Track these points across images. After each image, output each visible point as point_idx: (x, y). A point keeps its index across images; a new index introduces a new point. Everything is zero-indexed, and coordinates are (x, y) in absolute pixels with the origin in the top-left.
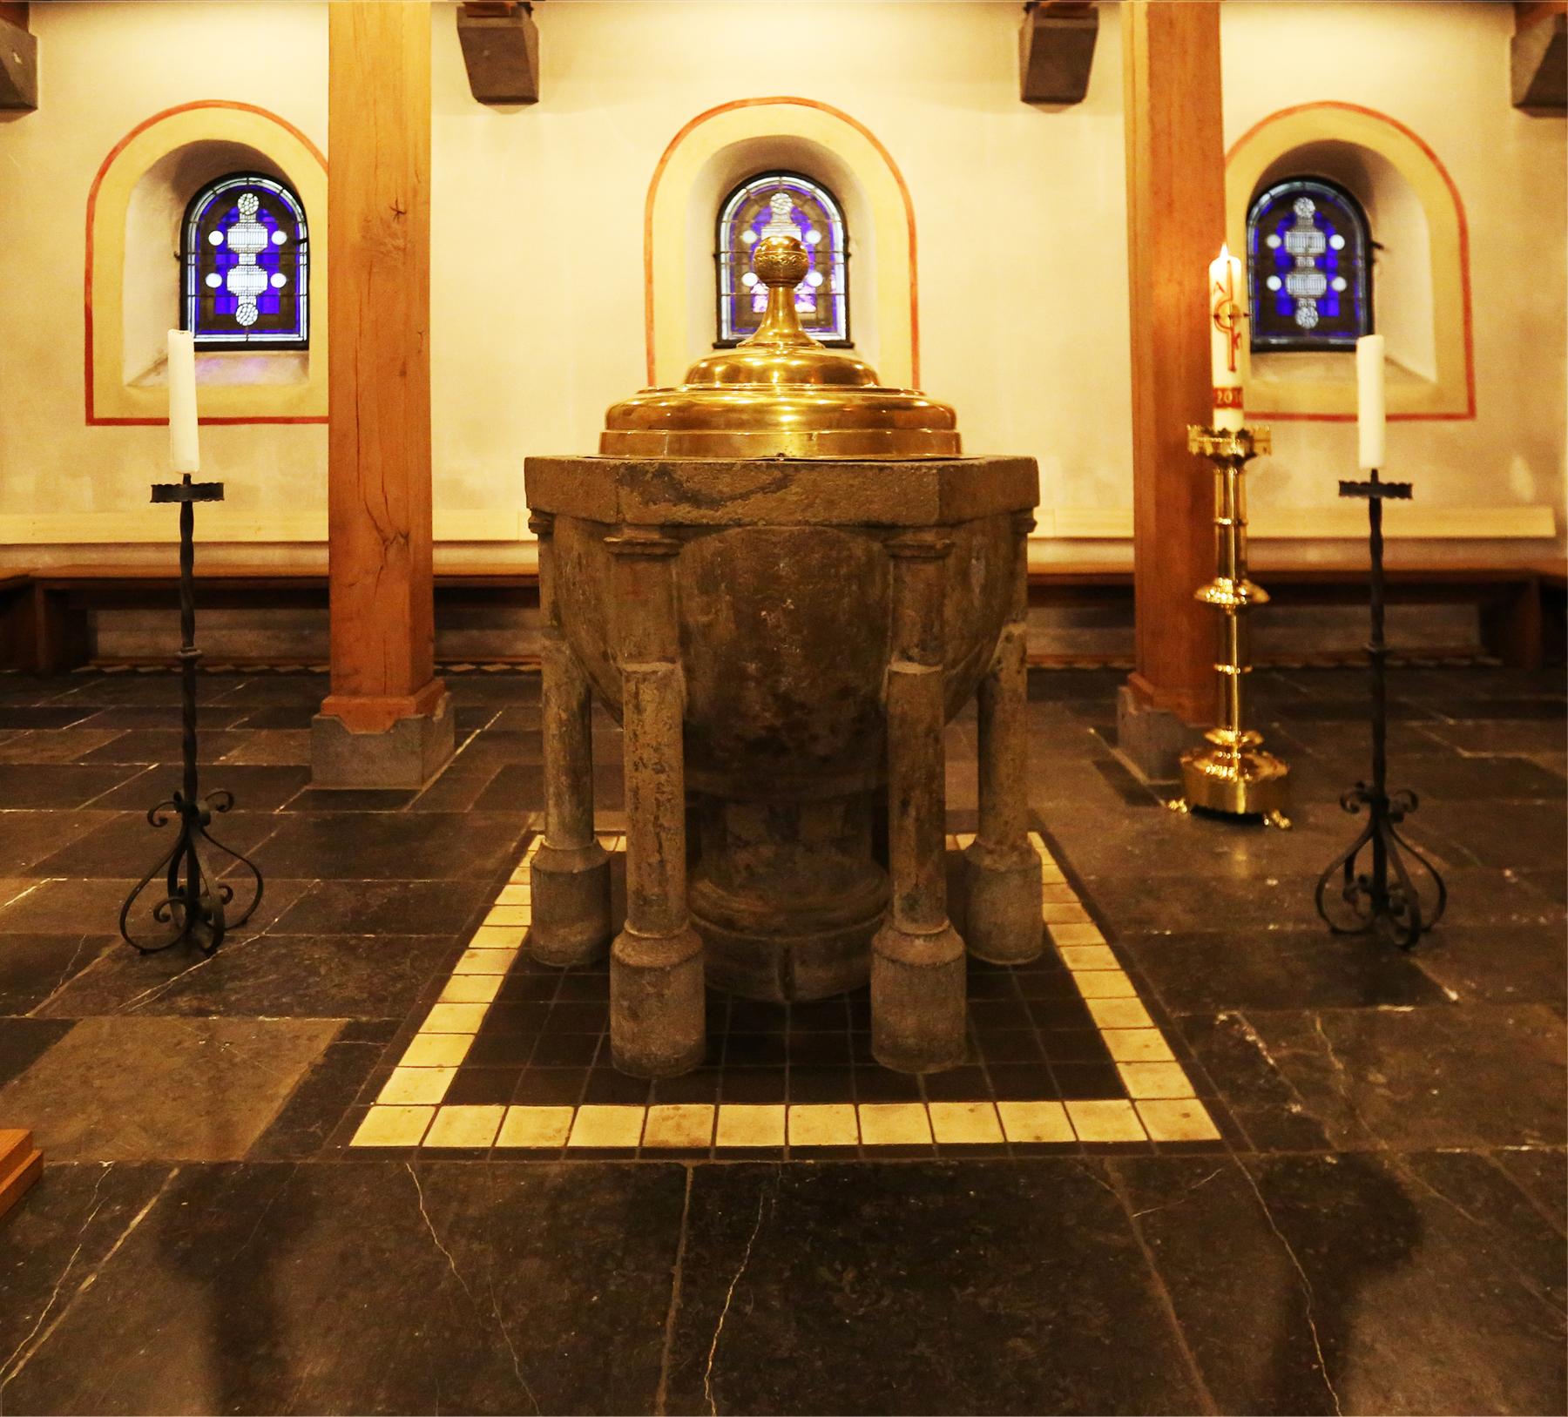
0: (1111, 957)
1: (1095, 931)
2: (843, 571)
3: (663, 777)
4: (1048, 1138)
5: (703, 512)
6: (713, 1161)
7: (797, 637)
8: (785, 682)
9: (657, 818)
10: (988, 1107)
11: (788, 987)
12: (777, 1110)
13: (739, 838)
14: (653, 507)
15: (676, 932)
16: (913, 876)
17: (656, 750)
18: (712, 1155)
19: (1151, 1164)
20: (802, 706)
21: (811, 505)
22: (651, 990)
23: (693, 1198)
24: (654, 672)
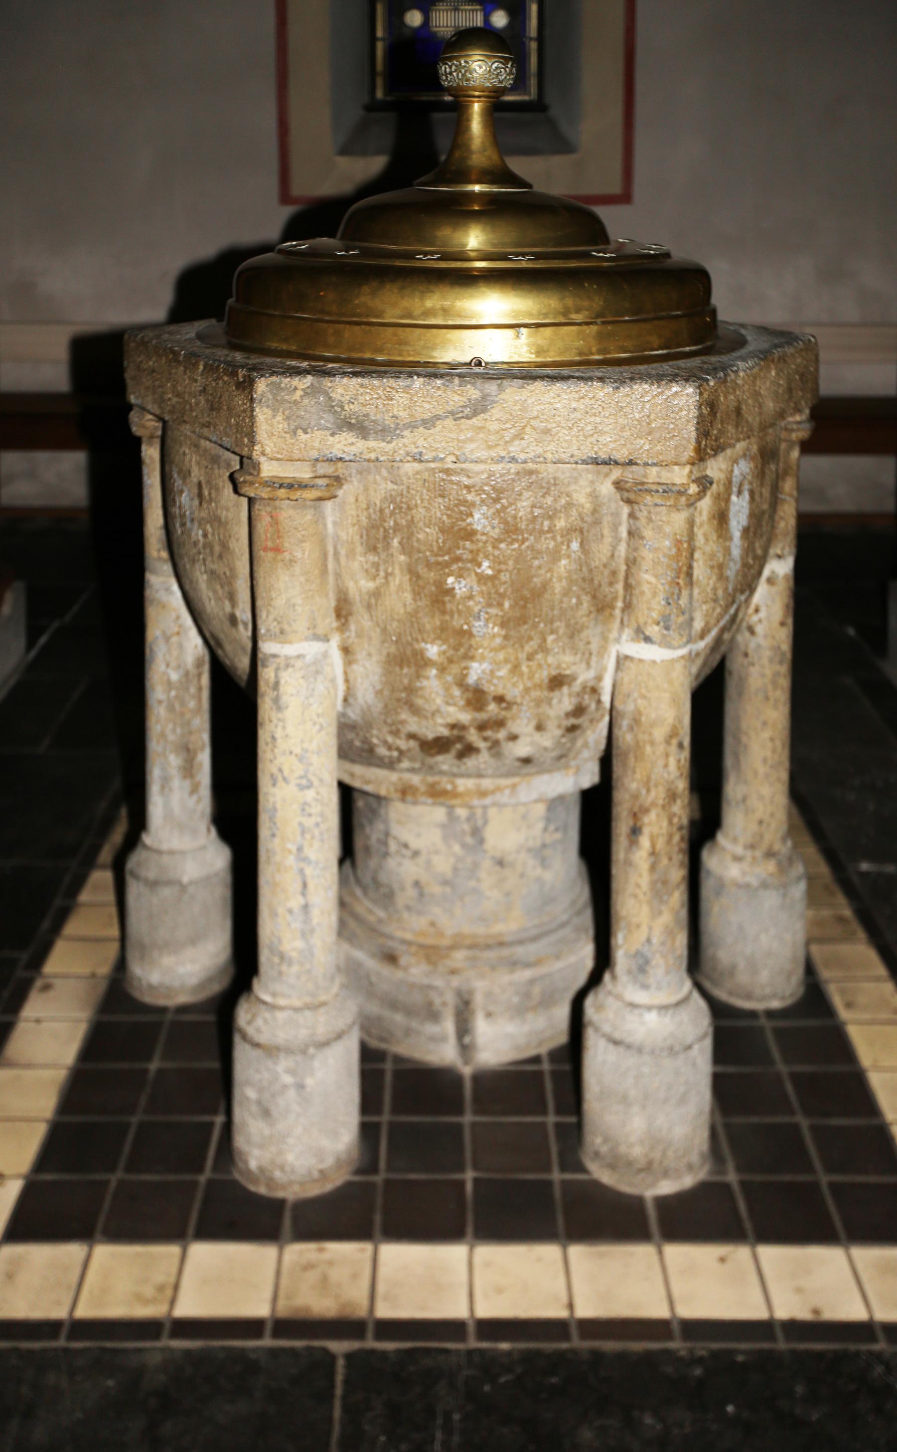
1: (871, 955)
2: (561, 523)
3: (310, 794)
5: (372, 444)
6: (371, 1344)
7: (493, 611)
9: (300, 849)
10: (741, 1253)
13: (406, 846)
14: (303, 437)
15: (323, 998)
17: (301, 759)
18: (370, 1333)
20: (500, 699)
21: (519, 436)
22: (288, 1079)
23: (346, 1408)
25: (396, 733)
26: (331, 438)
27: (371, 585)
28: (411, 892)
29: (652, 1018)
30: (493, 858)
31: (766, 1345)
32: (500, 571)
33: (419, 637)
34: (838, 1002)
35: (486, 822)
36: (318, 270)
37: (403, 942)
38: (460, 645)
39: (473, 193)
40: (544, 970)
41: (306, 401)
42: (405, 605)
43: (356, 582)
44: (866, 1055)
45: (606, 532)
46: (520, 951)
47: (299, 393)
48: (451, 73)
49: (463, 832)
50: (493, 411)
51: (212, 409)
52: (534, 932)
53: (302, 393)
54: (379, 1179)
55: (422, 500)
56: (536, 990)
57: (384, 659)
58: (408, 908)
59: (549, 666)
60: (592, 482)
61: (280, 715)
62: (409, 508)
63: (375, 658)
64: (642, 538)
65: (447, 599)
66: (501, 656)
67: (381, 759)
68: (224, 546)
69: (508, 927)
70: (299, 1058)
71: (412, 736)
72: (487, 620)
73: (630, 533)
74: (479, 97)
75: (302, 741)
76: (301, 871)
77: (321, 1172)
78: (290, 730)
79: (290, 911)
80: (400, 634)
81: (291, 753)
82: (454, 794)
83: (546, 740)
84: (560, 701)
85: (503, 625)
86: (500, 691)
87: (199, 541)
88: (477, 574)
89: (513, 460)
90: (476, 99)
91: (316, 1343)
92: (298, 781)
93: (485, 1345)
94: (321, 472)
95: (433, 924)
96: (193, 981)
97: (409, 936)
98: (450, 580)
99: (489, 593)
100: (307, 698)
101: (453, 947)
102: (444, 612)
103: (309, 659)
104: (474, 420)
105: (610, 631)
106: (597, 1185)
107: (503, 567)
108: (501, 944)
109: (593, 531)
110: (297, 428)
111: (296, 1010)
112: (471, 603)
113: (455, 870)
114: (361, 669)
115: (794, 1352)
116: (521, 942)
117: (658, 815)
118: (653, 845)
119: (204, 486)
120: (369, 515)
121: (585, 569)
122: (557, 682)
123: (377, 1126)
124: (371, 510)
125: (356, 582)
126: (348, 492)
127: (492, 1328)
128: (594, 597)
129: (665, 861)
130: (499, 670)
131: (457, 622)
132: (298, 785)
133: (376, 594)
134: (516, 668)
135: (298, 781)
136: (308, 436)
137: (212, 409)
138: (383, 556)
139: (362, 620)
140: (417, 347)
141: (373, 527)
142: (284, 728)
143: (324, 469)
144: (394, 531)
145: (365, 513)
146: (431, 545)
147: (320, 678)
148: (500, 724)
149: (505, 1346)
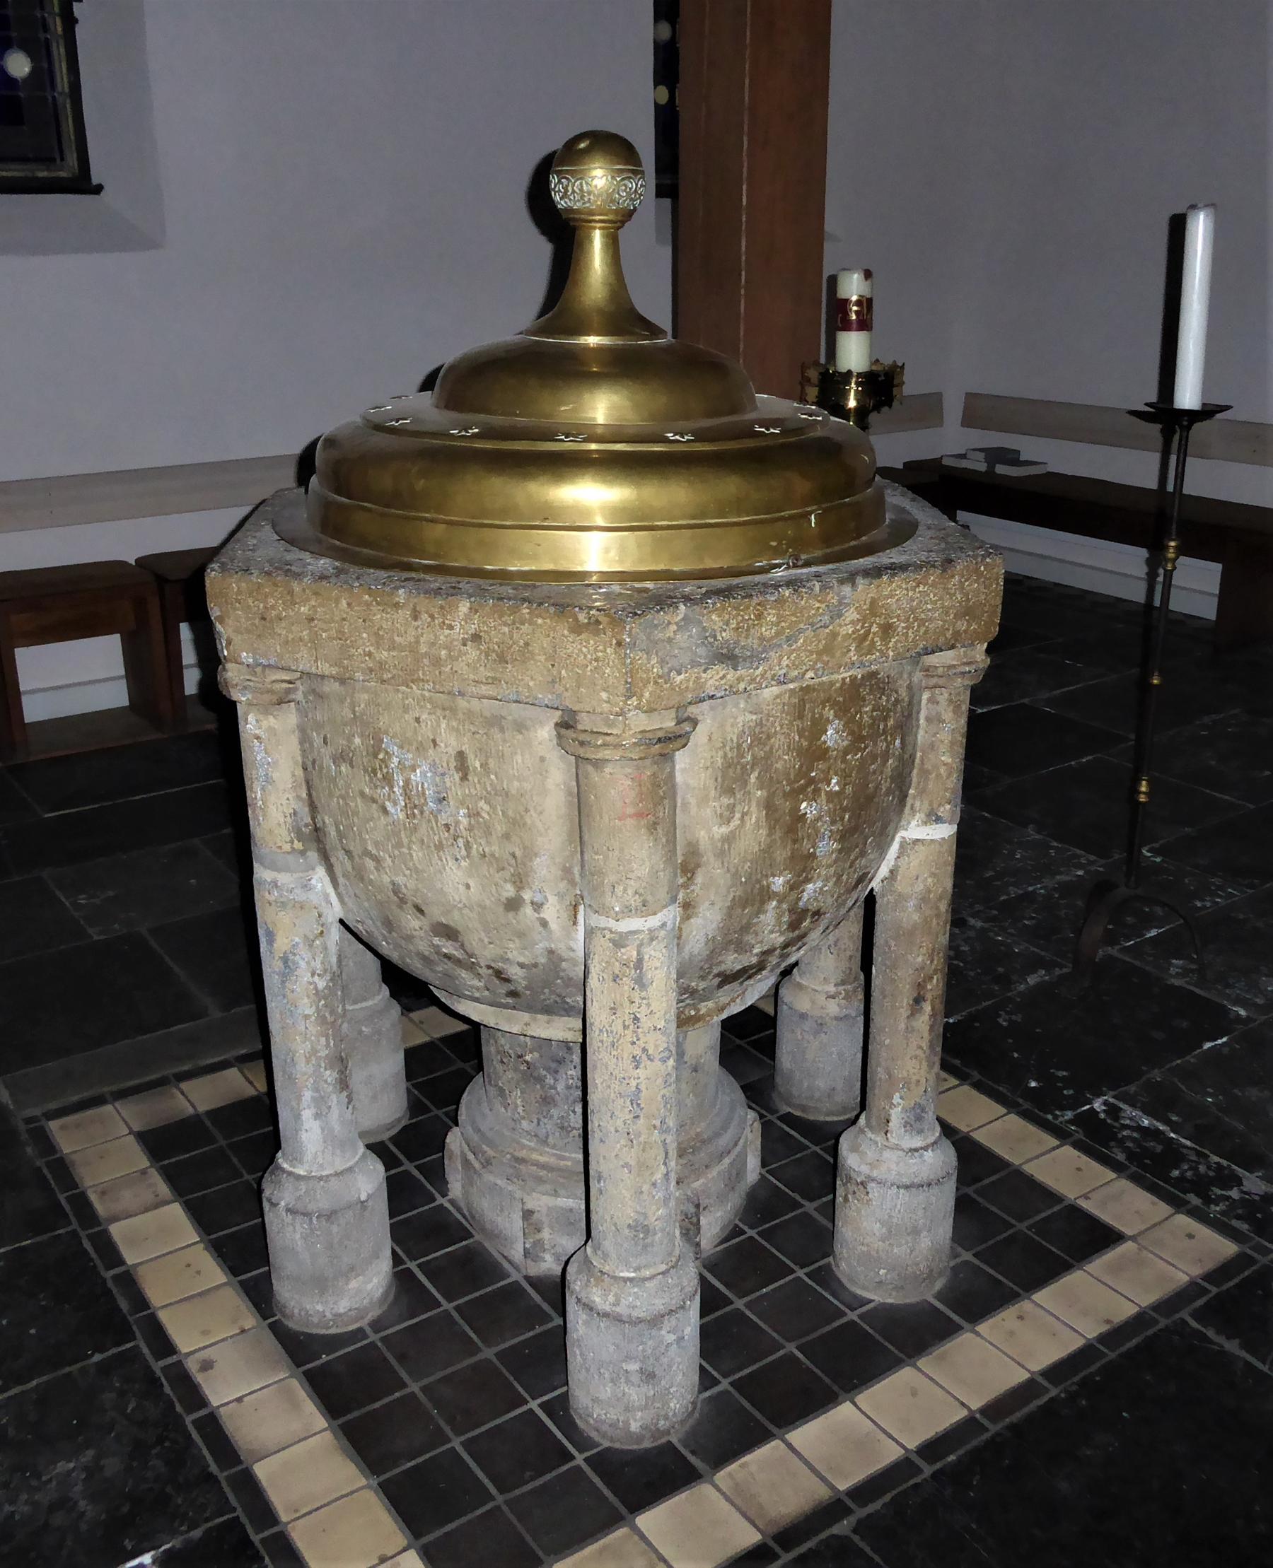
2: (891, 722)
10: (1025, 1305)
12: (844, 1411)
14: (679, 679)
19: (1248, 1298)
22: (671, 1338)
26: (704, 675)
27: (724, 830)
29: (929, 1155)
31: (1103, 1361)
36: (448, 458)
39: (586, 348)
51: (502, 659)
54: (725, 1384)
55: (781, 727)
61: (644, 994)
62: (769, 737)
63: (717, 907)
68: (516, 824)
81: (655, 1028)
89: (862, 665)
90: (598, 225)
93: (938, 1465)
96: (379, 1293)
98: (804, 805)
106: (885, 1309)
111: (663, 1273)
115: (1120, 1355)
116: (717, 1135)
120: (725, 754)
123: (159, 1356)
125: (709, 830)
126: (700, 736)
127: (931, 1449)
133: (729, 839)
136: (682, 676)
142: (648, 1005)
145: (721, 753)
146: (789, 774)
149: (952, 1458)
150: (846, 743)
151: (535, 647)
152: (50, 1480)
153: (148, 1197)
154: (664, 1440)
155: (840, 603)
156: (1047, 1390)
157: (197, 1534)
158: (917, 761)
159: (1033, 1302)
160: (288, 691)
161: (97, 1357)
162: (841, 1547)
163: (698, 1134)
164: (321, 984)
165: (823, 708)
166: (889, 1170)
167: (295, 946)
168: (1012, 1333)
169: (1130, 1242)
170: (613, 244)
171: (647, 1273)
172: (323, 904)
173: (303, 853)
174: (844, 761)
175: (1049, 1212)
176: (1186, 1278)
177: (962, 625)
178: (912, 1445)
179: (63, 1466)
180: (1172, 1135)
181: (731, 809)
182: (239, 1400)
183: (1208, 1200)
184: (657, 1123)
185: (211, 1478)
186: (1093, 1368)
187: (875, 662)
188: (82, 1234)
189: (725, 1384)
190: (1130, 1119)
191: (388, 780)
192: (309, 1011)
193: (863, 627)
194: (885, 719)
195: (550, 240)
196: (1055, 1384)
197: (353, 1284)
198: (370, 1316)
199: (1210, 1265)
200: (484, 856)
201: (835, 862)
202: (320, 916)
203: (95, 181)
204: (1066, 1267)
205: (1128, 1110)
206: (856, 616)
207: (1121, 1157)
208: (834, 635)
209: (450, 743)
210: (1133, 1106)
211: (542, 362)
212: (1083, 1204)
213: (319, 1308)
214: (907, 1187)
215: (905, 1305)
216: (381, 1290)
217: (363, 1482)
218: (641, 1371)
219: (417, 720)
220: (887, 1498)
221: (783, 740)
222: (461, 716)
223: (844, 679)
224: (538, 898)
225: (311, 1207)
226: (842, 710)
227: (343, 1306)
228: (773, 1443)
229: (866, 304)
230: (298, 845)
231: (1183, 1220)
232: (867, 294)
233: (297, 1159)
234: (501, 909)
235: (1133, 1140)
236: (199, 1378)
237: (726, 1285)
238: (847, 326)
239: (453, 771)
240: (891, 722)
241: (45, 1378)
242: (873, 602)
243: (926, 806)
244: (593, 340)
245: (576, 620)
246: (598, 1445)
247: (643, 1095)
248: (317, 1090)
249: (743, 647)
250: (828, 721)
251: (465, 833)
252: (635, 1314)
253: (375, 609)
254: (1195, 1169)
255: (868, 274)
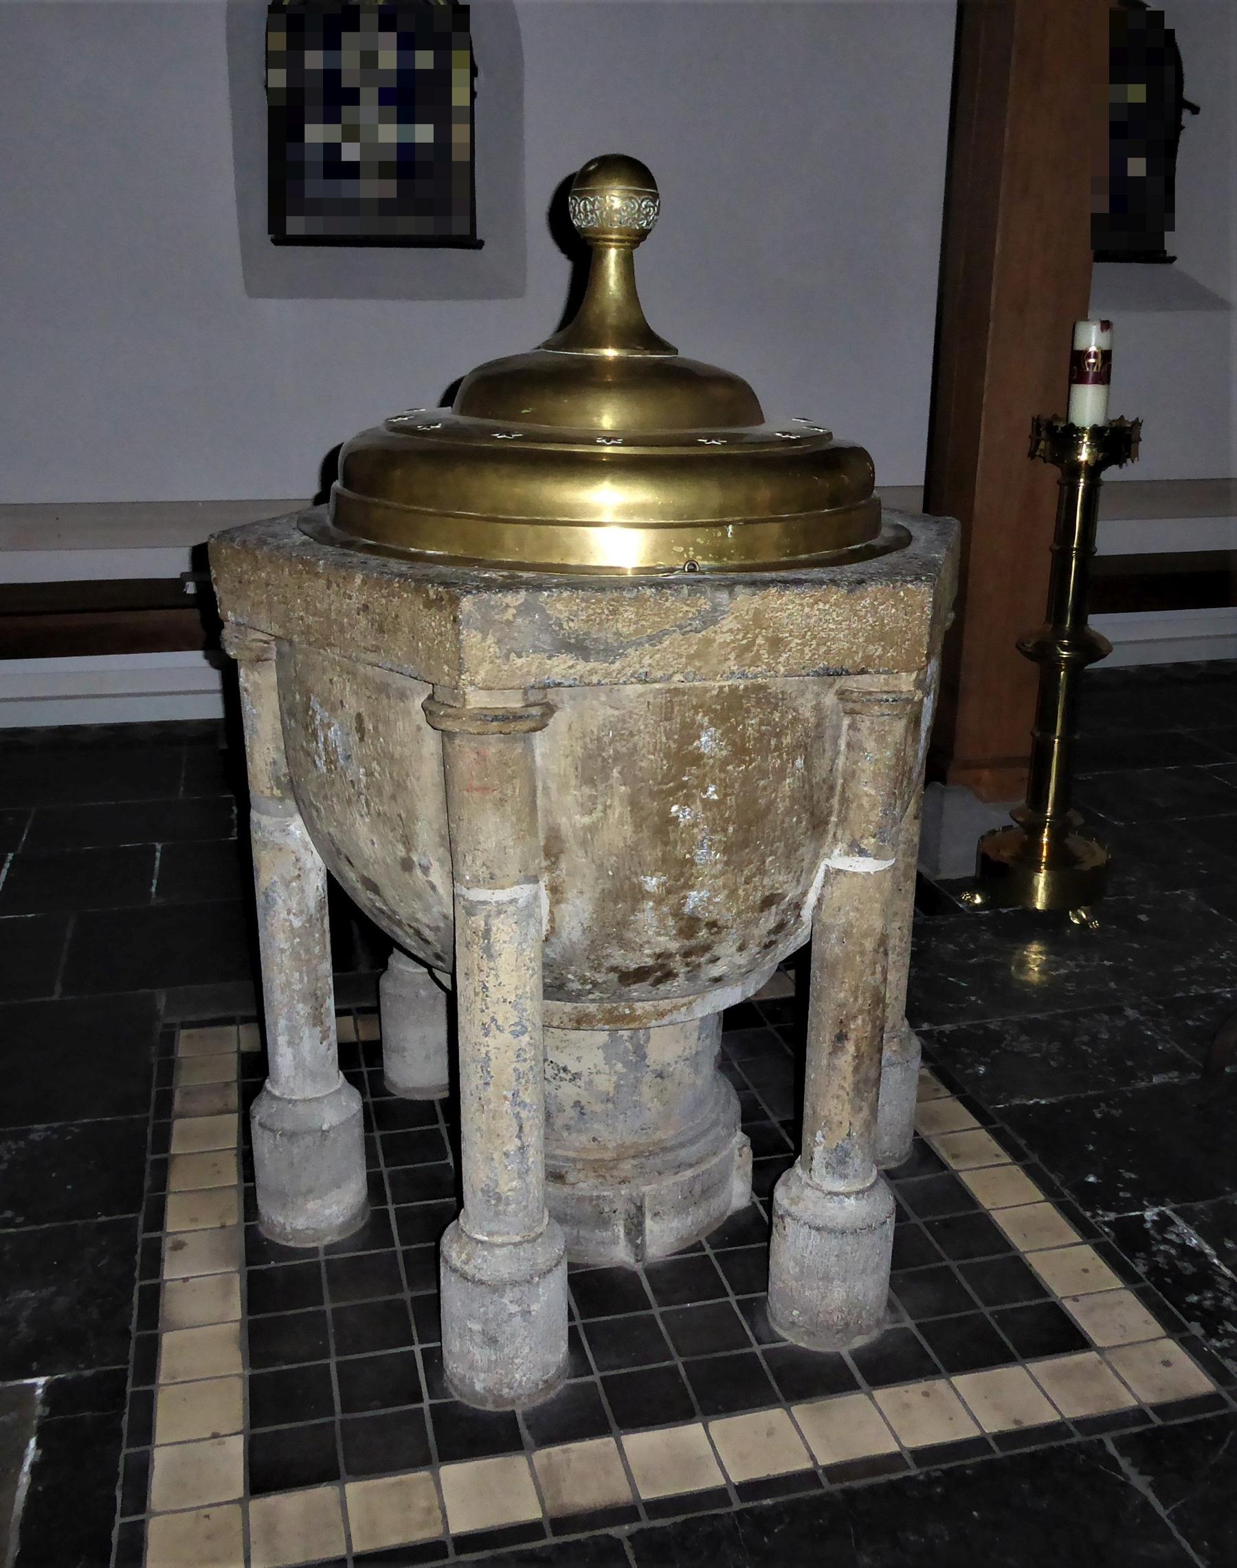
0: (995, 1146)
2: (787, 740)
4: (1029, 1422)
6: (646, 1523)
7: (716, 837)
8: (694, 898)
10: (940, 1385)
11: (639, 1250)
12: (694, 1430)
14: (519, 662)
16: (846, 1124)
17: (515, 1005)
19: (1163, 1437)
22: (514, 1308)
24: (513, 901)
25: (596, 968)
27: (586, 820)
28: (571, 1112)
29: (851, 1202)
30: (654, 1071)
31: (987, 1457)
32: (726, 795)
33: (639, 871)
34: (944, 1154)
35: (648, 1040)
37: (567, 1159)
38: (682, 874)
40: (704, 1167)
41: (519, 620)
42: (625, 838)
43: (570, 819)
44: (986, 1202)
45: (827, 746)
46: (683, 1154)
47: (512, 611)
48: (592, 211)
49: (626, 1051)
50: (724, 622)
51: (381, 630)
52: (691, 1134)
53: (515, 611)
54: (596, 1377)
56: (698, 1188)
57: (597, 895)
58: (568, 1128)
59: (764, 887)
60: (818, 694)
61: (492, 964)
62: (631, 734)
63: (587, 895)
64: (864, 750)
65: (671, 828)
66: (720, 882)
67: (569, 993)
68: (400, 786)
69: (665, 1135)
70: (525, 1288)
71: (613, 969)
72: (710, 847)
73: (849, 745)
74: (616, 241)
75: (516, 988)
76: (517, 1116)
77: (546, 1382)
78: (503, 978)
79: (506, 1154)
80: (617, 868)
82: (633, 1018)
83: (742, 959)
84: (767, 920)
85: (724, 852)
86: (715, 916)
87: (359, 780)
88: (702, 800)
89: (744, 675)
91: (598, 1532)
92: (513, 1028)
94: (532, 699)
95: (594, 1139)
97: (572, 1154)
98: (674, 808)
99: (714, 819)
100: (520, 944)
101: (618, 1159)
102: (666, 844)
103: (522, 903)
104: (703, 633)
105: (821, 847)
106: (794, 1351)
107: (729, 791)
108: (664, 1150)
109: (816, 746)
110: (510, 651)
111: (515, 1245)
112: (695, 830)
113: (618, 1087)
114: (570, 908)
116: (682, 1145)
117: (863, 1021)
118: (858, 1049)
119: (366, 719)
120: (585, 743)
121: (807, 786)
122: (768, 902)
124: (588, 740)
125: (570, 819)
126: (559, 721)
127: (750, 1489)
128: (812, 814)
129: (867, 1062)
130: (715, 896)
131: (680, 851)
132: (512, 1032)
133: (593, 829)
134: (733, 894)
135: (513, 1028)
136: (523, 660)
137: (381, 630)
138: (601, 787)
139: (575, 858)
140: (516, 544)
141: (590, 757)
142: (497, 976)
143: (534, 696)
144: (614, 760)
145: (580, 742)
146: (655, 773)
147: (532, 921)
148: (706, 948)
149: (768, 1502)
150: (724, 753)
151: (402, 619)
152: (10, 1302)
153: (219, 1104)
154: (509, 1408)
155: (714, 609)
156: (908, 1467)
157: (88, 1373)
158: (839, 788)
159: (951, 1383)
160: (264, 650)
161: (103, 1219)
162: (614, 1546)
163: (661, 1141)
164: (297, 923)
165: (697, 713)
166: (807, 1209)
167: (274, 883)
168: (907, 1406)
169: (1094, 1353)
170: (627, 262)
171: (499, 1240)
172: (302, 850)
173: (281, 800)
174: (722, 770)
175: (1026, 1303)
176: (1134, 1403)
177: (876, 650)
178: (736, 1479)
179: (26, 1294)
180: (1216, 1261)
181: (593, 799)
182: (185, 1280)
183: (1211, 1333)
184: (510, 1095)
185: (127, 1333)
186: (968, 1462)
187: (759, 673)
188: (151, 1122)
189: (596, 1377)
190: (1178, 1235)
191: (315, 735)
192: (285, 946)
193: (744, 638)
194: (778, 736)
195: (569, 258)
196: (919, 1465)
197: (311, 1205)
198: (328, 1240)
199: (1169, 1397)
200: (379, 814)
201: (723, 873)
202: (297, 860)
203: (478, 237)
204: (1006, 1358)
205: (1181, 1226)
206: (735, 625)
207: (1140, 1269)
208: (709, 642)
209: (353, 705)
210: (1189, 1222)
211: (558, 374)
212: (1069, 1305)
213: (281, 1220)
214: (818, 1229)
215: (816, 1353)
216: (341, 1219)
217: (240, 1370)
218: (483, 1332)
219: (331, 680)
220: (680, 1519)
221: (650, 739)
222: (359, 680)
223: (721, 688)
224: (424, 862)
225: (277, 1125)
226: (719, 718)
227: (300, 1223)
228: (606, 1439)
229: (1106, 356)
230: (277, 792)
231: (1171, 1347)
232: (1105, 347)
233: (275, 1082)
234: (399, 868)
235: (1166, 1254)
236: (167, 1254)
237: (654, 1291)
238: (1082, 379)
239: (354, 732)
240: (787, 740)
241: (54, 1225)
242: (758, 614)
243: (848, 836)
244: (611, 353)
245: (428, 595)
246: (452, 1396)
247: (492, 1064)
248: (290, 1020)
249: (595, 640)
250: (701, 726)
251: (364, 791)
252: (478, 1276)
253: (305, 576)
254: (1218, 1299)
255: (1106, 325)
